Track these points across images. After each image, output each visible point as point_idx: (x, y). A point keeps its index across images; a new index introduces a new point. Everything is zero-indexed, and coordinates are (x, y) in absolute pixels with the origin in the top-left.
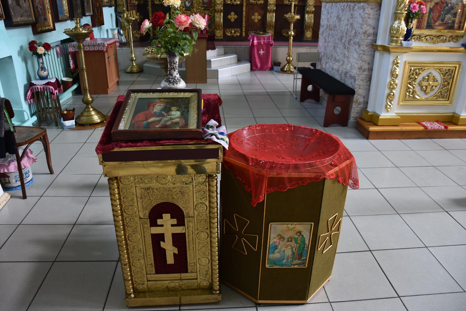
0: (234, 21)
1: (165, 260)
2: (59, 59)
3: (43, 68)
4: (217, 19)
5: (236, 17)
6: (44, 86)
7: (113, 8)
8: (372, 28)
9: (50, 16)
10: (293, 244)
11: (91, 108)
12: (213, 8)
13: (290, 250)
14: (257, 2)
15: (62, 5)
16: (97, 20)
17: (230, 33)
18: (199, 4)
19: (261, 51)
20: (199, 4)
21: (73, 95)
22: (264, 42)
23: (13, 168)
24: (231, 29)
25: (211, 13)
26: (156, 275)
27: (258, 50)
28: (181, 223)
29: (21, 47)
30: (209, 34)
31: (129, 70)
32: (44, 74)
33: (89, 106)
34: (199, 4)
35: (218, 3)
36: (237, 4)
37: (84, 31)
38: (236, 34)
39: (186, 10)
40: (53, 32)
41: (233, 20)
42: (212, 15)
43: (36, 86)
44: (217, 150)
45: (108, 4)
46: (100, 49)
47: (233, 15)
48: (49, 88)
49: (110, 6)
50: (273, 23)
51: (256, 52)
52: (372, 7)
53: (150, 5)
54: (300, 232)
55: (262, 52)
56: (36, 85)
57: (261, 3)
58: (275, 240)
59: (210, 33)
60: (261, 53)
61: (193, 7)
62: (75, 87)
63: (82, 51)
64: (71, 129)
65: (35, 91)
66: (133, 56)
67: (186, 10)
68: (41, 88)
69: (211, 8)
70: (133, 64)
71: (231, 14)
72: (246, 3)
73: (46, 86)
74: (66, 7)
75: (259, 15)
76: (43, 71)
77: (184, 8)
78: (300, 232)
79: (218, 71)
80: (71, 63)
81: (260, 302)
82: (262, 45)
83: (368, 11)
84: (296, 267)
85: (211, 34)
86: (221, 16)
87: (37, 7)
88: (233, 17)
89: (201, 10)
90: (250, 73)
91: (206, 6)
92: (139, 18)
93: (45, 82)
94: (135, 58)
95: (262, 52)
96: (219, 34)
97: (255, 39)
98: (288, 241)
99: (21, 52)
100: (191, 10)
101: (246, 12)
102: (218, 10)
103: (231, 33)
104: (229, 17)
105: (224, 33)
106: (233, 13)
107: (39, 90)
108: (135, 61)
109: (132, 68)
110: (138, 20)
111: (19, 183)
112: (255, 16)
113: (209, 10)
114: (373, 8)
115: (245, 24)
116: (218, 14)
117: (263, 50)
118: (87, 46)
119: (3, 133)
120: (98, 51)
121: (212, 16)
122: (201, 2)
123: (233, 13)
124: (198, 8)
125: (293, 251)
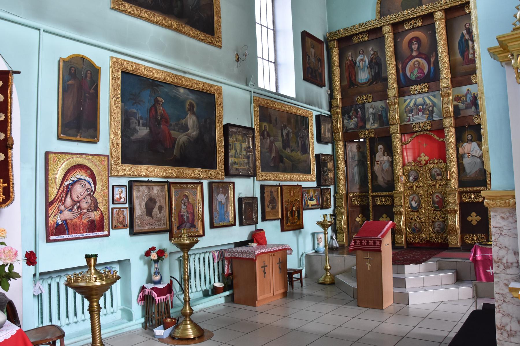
5: (479, 218)
8: (513, 253)
11: (189, 321)
17: (472, 240)
18: (428, 204)
21: (226, 302)
24: (472, 235)
30: (442, 240)
31: (321, 280)
33: (187, 319)
36: (478, 202)
39: (412, 211)
46: (251, 258)
52: (503, 215)
59: (444, 240)
61: (421, 207)
63: (186, 260)
64: (161, 339)
66: (328, 264)
67: (412, 211)
68: (148, 292)
69: (444, 208)
70: (327, 273)
71: (472, 215)
76: (155, 276)
83: (497, 223)
85: (445, 240)
89: (431, 210)
91: (437, 205)
92: (361, 220)
94: (329, 267)
97: (478, 252)
100: (418, 211)
104: (469, 219)
105: (462, 240)
106: (474, 214)
108: (329, 270)
109: (325, 278)
113: (441, 210)
114: (506, 217)
118: (245, 253)
120: (249, 259)
121: (446, 218)
122: (430, 201)
123: (474, 214)
124: (427, 208)
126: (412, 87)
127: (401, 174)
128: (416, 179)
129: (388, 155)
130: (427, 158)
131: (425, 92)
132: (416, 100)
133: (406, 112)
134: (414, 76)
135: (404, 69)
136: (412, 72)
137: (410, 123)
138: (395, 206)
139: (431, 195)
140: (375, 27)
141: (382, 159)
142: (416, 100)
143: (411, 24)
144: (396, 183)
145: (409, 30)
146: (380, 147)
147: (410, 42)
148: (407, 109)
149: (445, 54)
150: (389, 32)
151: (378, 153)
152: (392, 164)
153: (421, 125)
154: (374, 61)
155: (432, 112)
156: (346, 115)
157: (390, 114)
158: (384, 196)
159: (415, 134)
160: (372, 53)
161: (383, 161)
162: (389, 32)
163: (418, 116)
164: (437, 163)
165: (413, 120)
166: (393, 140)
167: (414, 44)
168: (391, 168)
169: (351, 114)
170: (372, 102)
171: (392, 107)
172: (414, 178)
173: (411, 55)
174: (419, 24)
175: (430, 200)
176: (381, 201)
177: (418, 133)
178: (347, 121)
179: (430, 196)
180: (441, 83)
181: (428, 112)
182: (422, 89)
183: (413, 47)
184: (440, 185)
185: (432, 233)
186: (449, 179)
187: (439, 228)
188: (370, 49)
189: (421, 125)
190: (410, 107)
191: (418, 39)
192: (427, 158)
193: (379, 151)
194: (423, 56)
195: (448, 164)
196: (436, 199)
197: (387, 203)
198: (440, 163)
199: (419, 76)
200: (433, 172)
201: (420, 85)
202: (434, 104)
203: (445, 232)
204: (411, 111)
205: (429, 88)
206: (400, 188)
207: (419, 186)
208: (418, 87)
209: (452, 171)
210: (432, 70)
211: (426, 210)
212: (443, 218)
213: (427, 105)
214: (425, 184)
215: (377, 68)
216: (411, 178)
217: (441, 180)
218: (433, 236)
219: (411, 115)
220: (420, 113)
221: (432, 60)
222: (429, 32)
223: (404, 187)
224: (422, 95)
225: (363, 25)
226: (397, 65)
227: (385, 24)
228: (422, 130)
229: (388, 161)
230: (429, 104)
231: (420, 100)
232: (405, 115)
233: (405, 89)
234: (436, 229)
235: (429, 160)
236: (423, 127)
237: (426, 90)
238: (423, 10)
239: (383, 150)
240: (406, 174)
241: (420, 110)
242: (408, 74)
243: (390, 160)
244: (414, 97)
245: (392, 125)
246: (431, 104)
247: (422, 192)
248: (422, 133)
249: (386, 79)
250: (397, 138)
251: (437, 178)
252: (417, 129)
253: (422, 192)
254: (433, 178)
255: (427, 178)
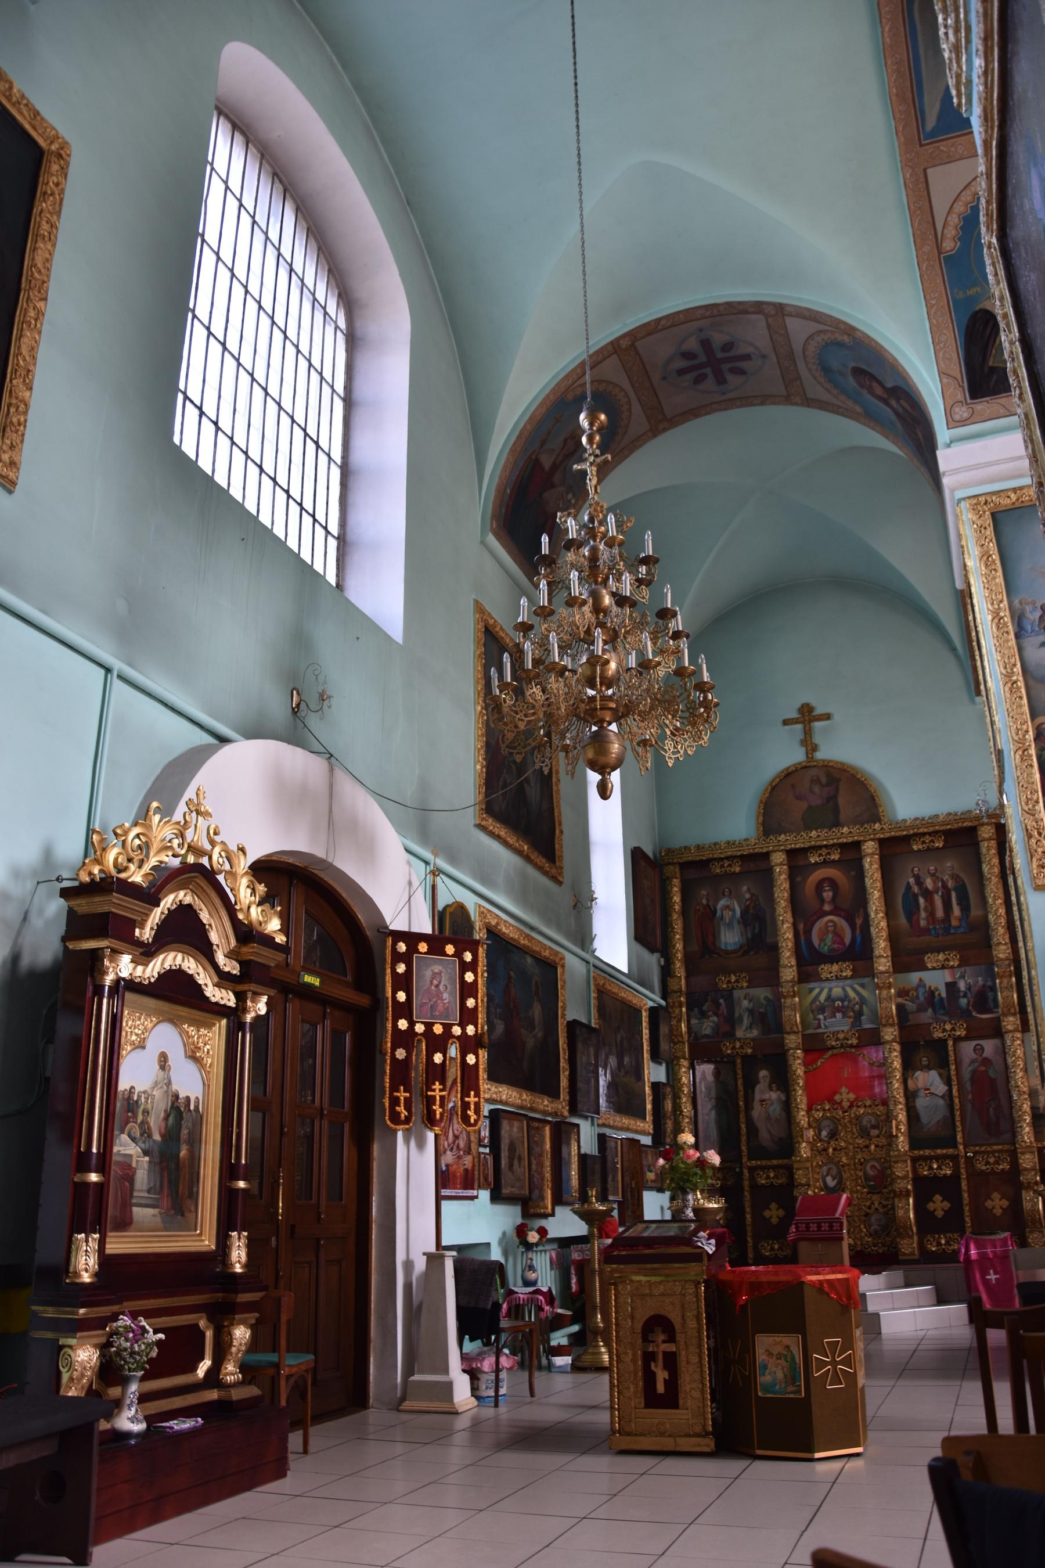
0: (943, 1216)
1: (655, 1389)
2: (553, 1272)
3: (531, 1268)
4: (900, 1213)
5: (946, 1205)
6: (529, 1296)
7: (668, 1194)
9: (549, 1192)
10: (782, 1362)
12: (890, 1188)
13: (781, 1371)
14: (992, 1168)
15: (569, 1179)
16: (629, 1213)
17: (937, 1246)
19: (996, 1279)
20: (856, 1180)
22: (994, 1252)
23: (487, 1366)
25: (887, 1199)
26: (645, 1410)
27: (984, 1273)
28: (671, 1339)
29: (504, 1233)
32: (532, 1276)
34: (856, 1180)
35: (899, 1177)
36: (945, 1175)
37: (601, 1208)
38: (952, 1247)
40: (550, 1218)
41: (940, 1214)
42: (887, 1205)
43: (516, 1295)
44: (701, 1254)
45: (654, 1185)
47: (939, 1202)
48: (538, 1299)
49: (660, 1190)
50: (1039, 1215)
51: (978, 1276)
53: (747, 1188)
54: (788, 1347)
55: (992, 1277)
56: (517, 1293)
57: (1003, 1170)
58: (764, 1357)
60: (991, 1279)
62: (575, 1328)
64: (562, 1370)
65: (514, 1304)
72: (967, 1172)
73: (533, 1296)
74: (575, 1182)
75: (1004, 1196)
77: (822, 1190)
78: (788, 1347)
79: (878, 1315)
80: (574, 1280)
81: (759, 1452)
82: (989, 1258)
84: (792, 1396)
86: (909, 1205)
87: (533, 1176)
88: (939, 1205)
89: (862, 1193)
90: (968, 1327)
93: (531, 1289)
95: (992, 1277)
96: (909, 1246)
97: (972, 1246)
98: (778, 1359)
99: (503, 1240)
101: (969, 1191)
102: (901, 1191)
103: (939, 1244)
104: (931, 1206)
105: (921, 1246)
106: (938, 1198)
107: (521, 1302)
110: (721, 1222)
111: (492, 1393)
112: (992, 1200)
113: (880, 1192)
115: (971, 1220)
116: (900, 1201)
117: (995, 1273)
119: (490, 1304)
123: (938, 1198)
125: (784, 1372)
126: (823, 966)
127: (806, 1126)
128: (833, 1135)
129: (778, 1089)
130: (852, 1096)
131: (846, 978)
132: (830, 990)
133: (812, 1011)
134: (826, 948)
135: (808, 932)
136: (822, 940)
137: (820, 1031)
138: (797, 1186)
139: (861, 1164)
140: (756, 851)
141: (767, 1096)
142: (830, 990)
143: (820, 855)
144: (798, 1142)
145: (816, 863)
146: (763, 1073)
147: (819, 886)
148: (814, 1006)
149: (881, 915)
150: (781, 864)
151: (758, 1086)
152: (788, 1106)
153: (841, 1036)
154: (751, 911)
155: (860, 1013)
156: (696, 1010)
157: (786, 1013)
158: (774, 1168)
159: (830, 1053)
160: (748, 896)
161: (769, 1100)
162: (781, 864)
163: (834, 1020)
164: (870, 1106)
165: (826, 1027)
166: (791, 1062)
167: (825, 891)
168: (784, 1114)
169: (705, 1008)
170: (748, 987)
171: (789, 1001)
172: (828, 1134)
173: (821, 909)
174: (835, 856)
175: (860, 1174)
176: (768, 1177)
177: (835, 1051)
178: (697, 1021)
179: (859, 1167)
180: (875, 965)
181: (851, 1014)
182: (842, 971)
183: (825, 894)
184: (877, 1146)
185: (866, 1235)
186: (894, 1134)
187: (879, 1225)
188: (745, 888)
189: (841, 1036)
190: (820, 1002)
191: (833, 883)
192: (852, 1096)
193: (762, 1081)
194: (843, 914)
195: (891, 1107)
196: (871, 1173)
197: (779, 1181)
198: (836, 1109)
199: (834, 949)
200: (865, 1122)
201: (837, 963)
202: (863, 1001)
203: (889, 1233)
204: (822, 1009)
205: (854, 970)
206: (804, 1150)
207: (839, 1148)
208: (835, 967)
209: (899, 1120)
210: (859, 940)
211: (854, 1192)
212: (884, 1206)
213: (850, 1001)
214: (850, 1144)
215: (757, 925)
216: (824, 1133)
217: (878, 1136)
218: (868, 1242)
219: (821, 1017)
220: (839, 1015)
221: (859, 922)
222: (853, 873)
223: (812, 1150)
224: (841, 983)
225: (734, 844)
226: (795, 925)
227: (776, 848)
228: (842, 1046)
229: (779, 1099)
230: (854, 998)
231: (837, 991)
232: (811, 1016)
233: (810, 968)
234: (872, 1228)
235: (856, 1099)
236: (843, 1039)
237: (849, 973)
238: (844, 835)
239: (768, 1080)
240: (814, 1125)
241: (838, 1010)
242: (816, 941)
243: (783, 1098)
244: (827, 984)
245: (788, 1033)
246: (857, 999)
247: (844, 1160)
248: (842, 1050)
249: (774, 949)
250: (798, 1057)
251: (872, 1134)
252: (834, 1043)
253: (844, 1160)
254: (864, 1133)
255: (853, 1134)
